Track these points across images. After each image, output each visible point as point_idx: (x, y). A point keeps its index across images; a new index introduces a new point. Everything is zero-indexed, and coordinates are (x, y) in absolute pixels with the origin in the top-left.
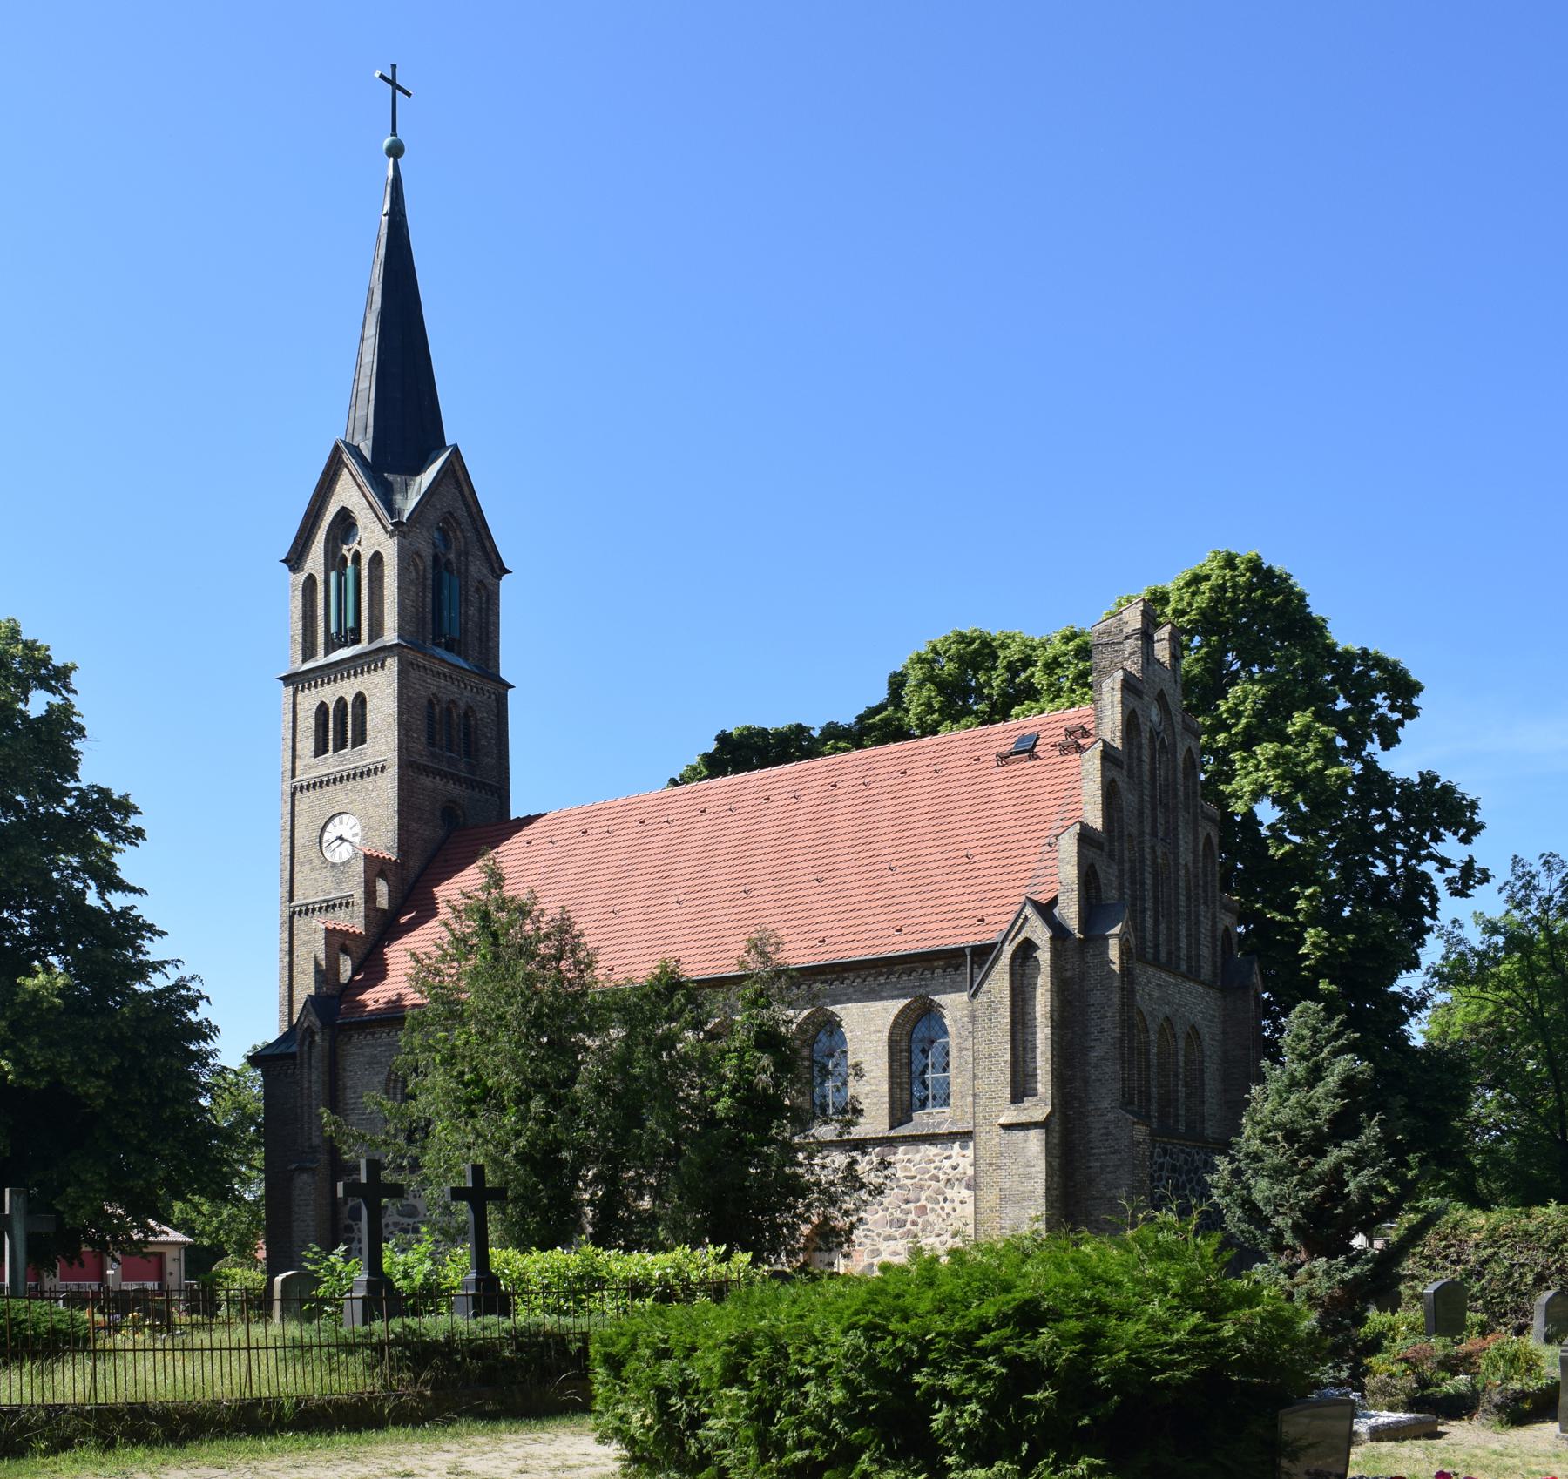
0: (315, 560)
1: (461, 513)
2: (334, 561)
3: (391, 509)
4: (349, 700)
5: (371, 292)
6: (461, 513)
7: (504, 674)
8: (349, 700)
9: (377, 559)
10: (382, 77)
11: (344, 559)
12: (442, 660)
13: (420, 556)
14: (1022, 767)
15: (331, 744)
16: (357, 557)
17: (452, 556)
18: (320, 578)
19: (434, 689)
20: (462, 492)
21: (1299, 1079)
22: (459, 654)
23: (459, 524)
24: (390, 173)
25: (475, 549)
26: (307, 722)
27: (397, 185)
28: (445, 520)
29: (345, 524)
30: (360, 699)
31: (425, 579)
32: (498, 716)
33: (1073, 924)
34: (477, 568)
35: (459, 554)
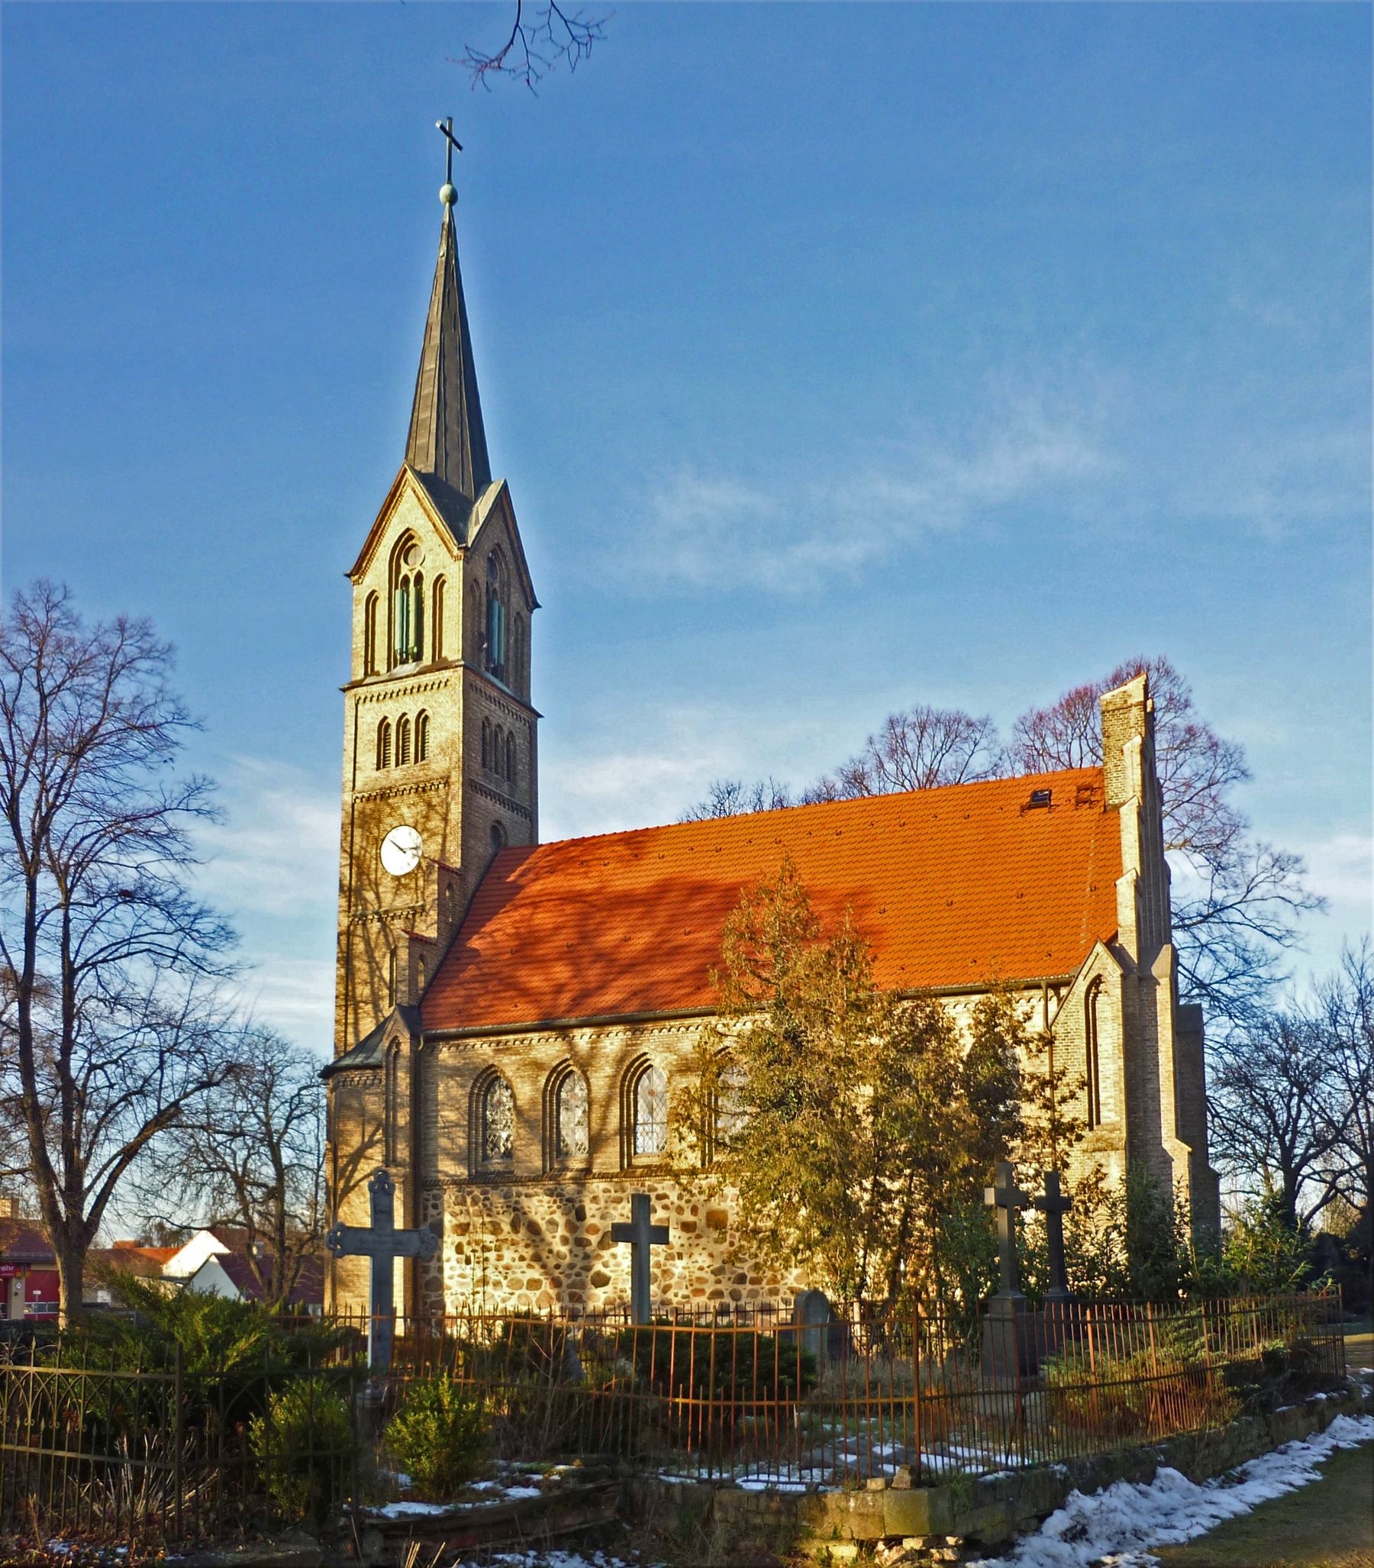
0: (377, 575)
1: (506, 546)
2: (397, 581)
3: (460, 537)
4: (412, 717)
5: (428, 327)
6: (506, 546)
7: (534, 704)
8: (412, 717)
9: (439, 582)
10: (442, 127)
11: (406, 579)
12: (493, 685)
13: (477, 583)
14: (1040, 813)
15: (393, 758)
16: (419, 578)
17: (497, 585)
18: (383, 595)
19: (487, 712)
20: (507, 525)
21: (837, 1171)
22: (502, 680)
23: (504, 556)
24: (447, 220)
25: (515, 581)
26: (369, 735)
27: (451, 231)
28: (493, 552)
29: (406, 545)
30: (423, 719)
31: (480, 604)
32: (530, 743)
33: (1132, 951)
34: (516, 600)
35: (502, 586)
